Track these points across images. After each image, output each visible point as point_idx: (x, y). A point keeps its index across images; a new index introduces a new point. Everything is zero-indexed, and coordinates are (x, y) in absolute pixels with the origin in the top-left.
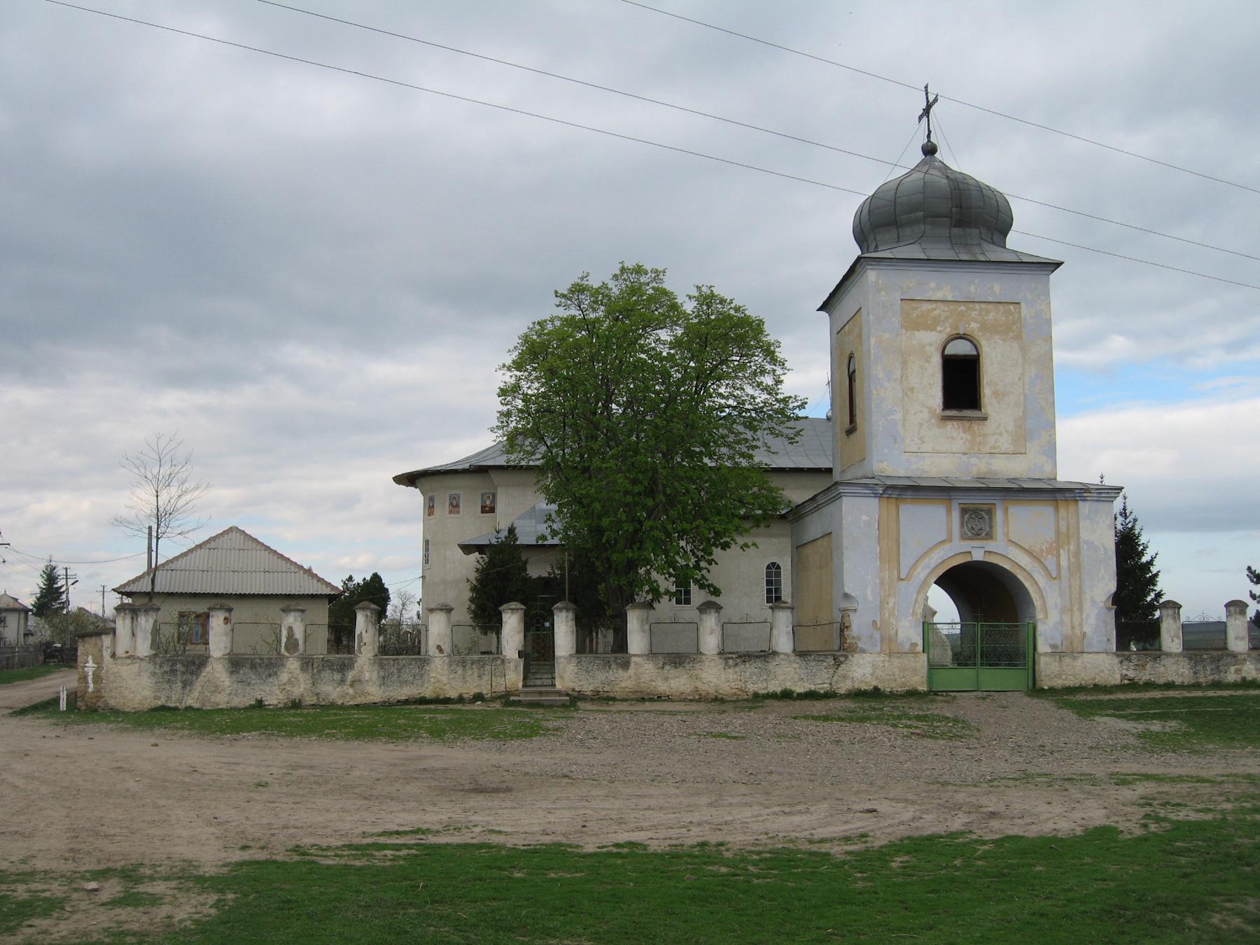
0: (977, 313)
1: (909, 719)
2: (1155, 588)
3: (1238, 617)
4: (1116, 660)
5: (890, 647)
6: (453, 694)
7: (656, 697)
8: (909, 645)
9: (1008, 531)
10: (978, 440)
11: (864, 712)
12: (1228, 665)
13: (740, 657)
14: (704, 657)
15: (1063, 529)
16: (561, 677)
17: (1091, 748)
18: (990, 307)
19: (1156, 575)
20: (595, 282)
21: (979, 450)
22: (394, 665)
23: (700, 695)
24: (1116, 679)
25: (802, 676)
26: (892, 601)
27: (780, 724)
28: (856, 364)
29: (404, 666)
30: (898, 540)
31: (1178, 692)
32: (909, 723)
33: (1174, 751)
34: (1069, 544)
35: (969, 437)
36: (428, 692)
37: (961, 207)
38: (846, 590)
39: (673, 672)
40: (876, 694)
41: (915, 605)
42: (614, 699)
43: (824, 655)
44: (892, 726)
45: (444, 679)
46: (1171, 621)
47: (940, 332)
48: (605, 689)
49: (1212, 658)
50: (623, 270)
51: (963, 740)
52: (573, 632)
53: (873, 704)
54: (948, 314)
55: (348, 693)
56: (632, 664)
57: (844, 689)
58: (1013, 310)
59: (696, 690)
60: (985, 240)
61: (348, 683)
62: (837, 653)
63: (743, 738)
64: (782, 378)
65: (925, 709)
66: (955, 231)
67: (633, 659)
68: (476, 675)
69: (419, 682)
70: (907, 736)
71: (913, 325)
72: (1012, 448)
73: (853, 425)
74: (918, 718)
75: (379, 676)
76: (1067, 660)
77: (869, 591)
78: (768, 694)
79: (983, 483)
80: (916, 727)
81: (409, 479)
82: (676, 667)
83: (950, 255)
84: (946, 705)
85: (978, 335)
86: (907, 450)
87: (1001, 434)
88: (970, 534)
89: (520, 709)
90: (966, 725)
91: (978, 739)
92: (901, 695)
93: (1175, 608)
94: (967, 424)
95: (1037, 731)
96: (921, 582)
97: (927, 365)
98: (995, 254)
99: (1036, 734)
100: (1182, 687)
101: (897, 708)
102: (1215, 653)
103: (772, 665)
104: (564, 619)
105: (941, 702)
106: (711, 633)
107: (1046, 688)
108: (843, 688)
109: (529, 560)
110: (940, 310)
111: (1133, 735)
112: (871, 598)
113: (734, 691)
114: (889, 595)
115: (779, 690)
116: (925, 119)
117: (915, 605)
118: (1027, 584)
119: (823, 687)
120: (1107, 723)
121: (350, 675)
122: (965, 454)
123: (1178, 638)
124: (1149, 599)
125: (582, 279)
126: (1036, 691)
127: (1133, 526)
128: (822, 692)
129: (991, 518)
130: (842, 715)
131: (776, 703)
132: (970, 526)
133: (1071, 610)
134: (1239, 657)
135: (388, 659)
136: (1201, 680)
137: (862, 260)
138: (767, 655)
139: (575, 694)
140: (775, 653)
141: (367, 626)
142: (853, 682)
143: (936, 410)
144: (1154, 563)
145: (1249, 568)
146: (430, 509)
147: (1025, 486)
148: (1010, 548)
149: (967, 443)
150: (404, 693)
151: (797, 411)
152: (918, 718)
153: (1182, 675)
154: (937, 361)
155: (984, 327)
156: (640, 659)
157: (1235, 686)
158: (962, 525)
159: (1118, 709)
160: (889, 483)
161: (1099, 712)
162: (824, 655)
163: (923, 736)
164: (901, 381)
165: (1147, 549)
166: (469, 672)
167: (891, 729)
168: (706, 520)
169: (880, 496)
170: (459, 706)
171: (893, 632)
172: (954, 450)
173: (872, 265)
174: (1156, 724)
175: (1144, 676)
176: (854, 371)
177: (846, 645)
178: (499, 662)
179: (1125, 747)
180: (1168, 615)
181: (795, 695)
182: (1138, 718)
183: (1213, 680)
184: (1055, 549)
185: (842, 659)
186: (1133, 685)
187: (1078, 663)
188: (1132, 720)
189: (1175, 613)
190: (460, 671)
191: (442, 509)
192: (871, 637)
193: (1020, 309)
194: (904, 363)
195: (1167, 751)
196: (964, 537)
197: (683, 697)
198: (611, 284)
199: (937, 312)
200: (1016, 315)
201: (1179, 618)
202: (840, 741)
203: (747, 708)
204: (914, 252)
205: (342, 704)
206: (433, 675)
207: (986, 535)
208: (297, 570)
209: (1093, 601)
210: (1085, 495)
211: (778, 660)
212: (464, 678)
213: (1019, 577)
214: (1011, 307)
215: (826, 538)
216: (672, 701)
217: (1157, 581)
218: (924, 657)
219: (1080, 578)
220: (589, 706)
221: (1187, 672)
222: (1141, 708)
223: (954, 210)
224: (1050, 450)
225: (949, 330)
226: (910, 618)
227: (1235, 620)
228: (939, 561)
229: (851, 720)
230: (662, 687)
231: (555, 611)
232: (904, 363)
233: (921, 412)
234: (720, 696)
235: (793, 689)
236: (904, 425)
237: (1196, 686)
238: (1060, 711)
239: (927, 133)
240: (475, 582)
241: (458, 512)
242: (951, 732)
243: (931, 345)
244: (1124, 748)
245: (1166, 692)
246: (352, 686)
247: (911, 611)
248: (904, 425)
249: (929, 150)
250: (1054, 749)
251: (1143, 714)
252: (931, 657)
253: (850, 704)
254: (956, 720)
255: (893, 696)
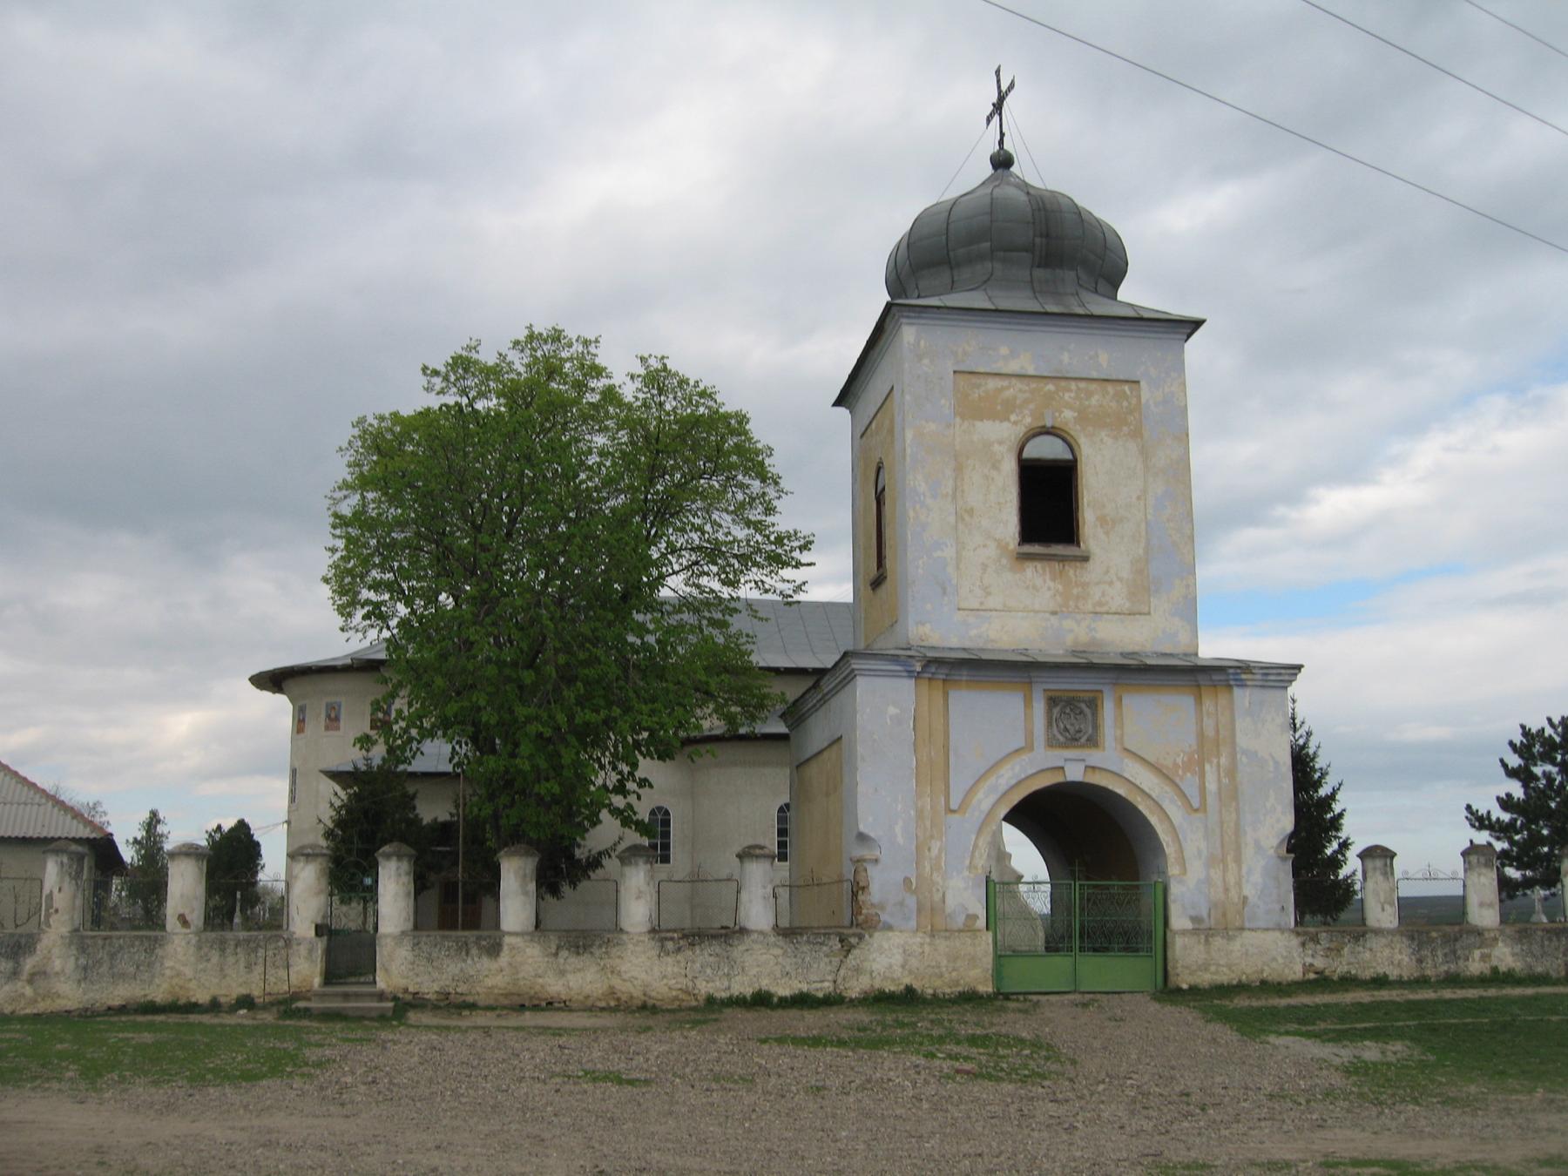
0: (1073, 395)
1: (958, 1043)
2: (1339, 835)
3: (1484, 870)
4: (1295, 942)
5: (932, 919)
6: (202, 997)
7: (544, 1004)
8: (963, 917)
9: (1122, 735)
10: (1075, 591)
11: (884, 1029)
12: (1470, 947)
13: (685, 937)
14: (625, 937)
15: (1210, 732)
16: (386, 970)
17: (1271, 1097)
18: (1093, 386)
19: (1341, 815)
20: (488, 357)
21: (1077, 607)
22: (103, 948)
23: (618, 999)
24: (1295, 972)
25: (788, 968)
26: (936, 846)
27: (733, 1052)
28: (886, 477)
29: (121, 948)
30: (946, 747)
31: (1394, 993)
32: (956, 1049)
33: (1416, 1101)
34: (1218, 756)
35: (1060, 587)
36: (159, 994)
37: (1047, 236)
38: (862, 828)
39: (574, 961)
40: (909, 998)
41: (973, 852)
42: (473, 1006)
43: (825, 934)
44: (926, 1056)
45: (188, 972)
46: (1380, 878)
47: (1015, 423)
48: (459, 990)
49: (1444, 936)
50: (531, 337)
51: (1046, 1083)
52: (409, 894)
53: (901, 1016)
54: (1027, 395)
55: (23, 995)
56: (505, 948)
57: (858, 989)
58: (1128, 392)
59: (612, 992)
60: (1087, 289)
61: (25, 976)
62: (845, 931)
63: (647, 1082)
64: (775, 503)
65: (987, 1025)
66: (1040, 273)
67: (507, 940)
68: (242, 964)
69: (146, 976)
70: (948, 1077)
71: (973, 411)
72: (1128, 605)
73: (881, 570)
74: (973, 1041)
75: (77, 966)
76: (1218, 942)
77: (898, 829)
78: (730, 998)
79: (1082, 658)
80: (966, 1058)
81: (273, 681)
82: (578, 954)
83: (1032, 305)
84: (1021, 1016)
85: (1074, 430)
86: (962, 605)
87: (1111, 583)
88: (1062, 739)
89: (305, 1023)
90: (1052, 1053)
91: (1071, 1080)
92: (950, 1000)
93: (1386, 857)
94: (1057, 566)
95: (1173, 1063)
96: (983, 816)
97: (994, 473)
98: (1099, 306)
99: (1173, 1068)
100: (1400, 983)
101: (940, 1022)
102: (1448, 929)
103: (738, 951)
104: (393, 873)
105: (1014, 1011)
106: (638, 898)
107: (1185, 986)
108: (855, 989)
109: (418, 795)
110: (1015, 389)
111: (1337, 1069)
112: (900, 840)
113: (674, 993)
114: (932, 837)
115: (748, 991)
116: (996, 118)
117: (973, 852)
118: (1153, 820)
119: (822, 988)
120: (1290, 1047)
121: (29, 964)
122: (1054, 613)
123: (1391, 904)
124: (1329, 851)
125: (469, 348)
126: (1168, 992)
127: (1305, 744)
128: (820, 995)
129: (1095, 714)
130: (844, 1036)
131: (740, 1013)
132: (1062, 726)
133: (1223, 861)
134: (1487, 935)
135: (94, 937)
136: (1428, 972)
137: (894, 309)
138: (732, 933)
139: (409, 997)
140: (743, 931)
141: (62, 881)
142: (872, 978)
143: (1008, 544)
144: (1337, 797)
145: (1469, 808)
146: (300, 724)
147: (1150, 662)
148: (1126, 760)
149: (1058, 597)
150: (120, 993)
151: (796, 554)
152: (973, 1041)
153: (1399, 964)
154: (1010, 468)
155: (1083, 417)
156: (519, 940)
157: (1482, 981)
158: (1049, 724)
159: (1305, 1022)
160: (930, 654)
161: (1274, 1028)
162: (825, 934)
163: (973, 1076)
164: (954, 497)
165: (1327, 777)
166: (231, 960)
167: (922, 1061)
168: (627, 710)
169: (918, 677)
170: (206, 1019)
171: (937, 897)
172: (1037, 607)
173: (908, 317)
174: (1370, 1048)
175: (1340, 966)
176: (884, 489)
177: (861, 918)
178: (281, 943)
179: (1329, 1093)
180: (1375, 869)
181: (775, 1000)
182: (1339, 1037)
183: (1447, 972)
184: (1197, 763)
185: (853, 940)
186: (1321, 982)
187: (1236, 946)
188: (1329, 1041)
189: (1386, 865)
190: (215, 957)
191: (316, 724)
192: (901, 904)
193: (1139, 390)
194: (959, 470)
195: (1403, 1100)
196: (1051, 743)
197: (589, 1003)
198: (514, 356)
199: (1009, 393)
200: (1134, 401)
201: (1392, 874)
202: (824, 1088)
203: (688, 1022)
204: (978, 300)
205: (13, 1013)
206: (168, 963)
207: (1088, 740)
208: (44, 801)
209: (1258, 847)
210: (1244, 676)
211: (747, 940)
212: (222, 970)
213: (1141, 808)
214: (1126, 388)
215: (835, 747)
216: (571, 1010)
217: (1341, 825)
218: (988, 937)
219: (1237, 810)
220: (426, 1018)
221: (1407, 959)
222: (1342, 1020)
223: (1038, 240)
224: (1188, 610)
225: (1028, 420)
226: (966, 873)
227: (1479, 875)
228: (1013, 782)
229: (857, 1044)
230: (554, 986)
231: (380, 860)
232: (959, 470)
233: (985, 546)
234: (650, 1002)
235: (773, 989)
236: (958, 568)
237: (1422, 982)
238: (1211, 1026)
239: (998, 138)
240: (331, 825)
241: (338, 728)
242: (1026, 1066)
243: (1000, 443)
244: (1327, 1095)
245: (1376, 993)
246: (30, 981)
247: (967, 862)
248: (958, 568)
249: (1002, 162)
250: (1208, 1100)
251: (1346, 1031)
252: (999, 937)
253: (863, 1016)
254: (1036, 1045)
255: (938, 1001)
